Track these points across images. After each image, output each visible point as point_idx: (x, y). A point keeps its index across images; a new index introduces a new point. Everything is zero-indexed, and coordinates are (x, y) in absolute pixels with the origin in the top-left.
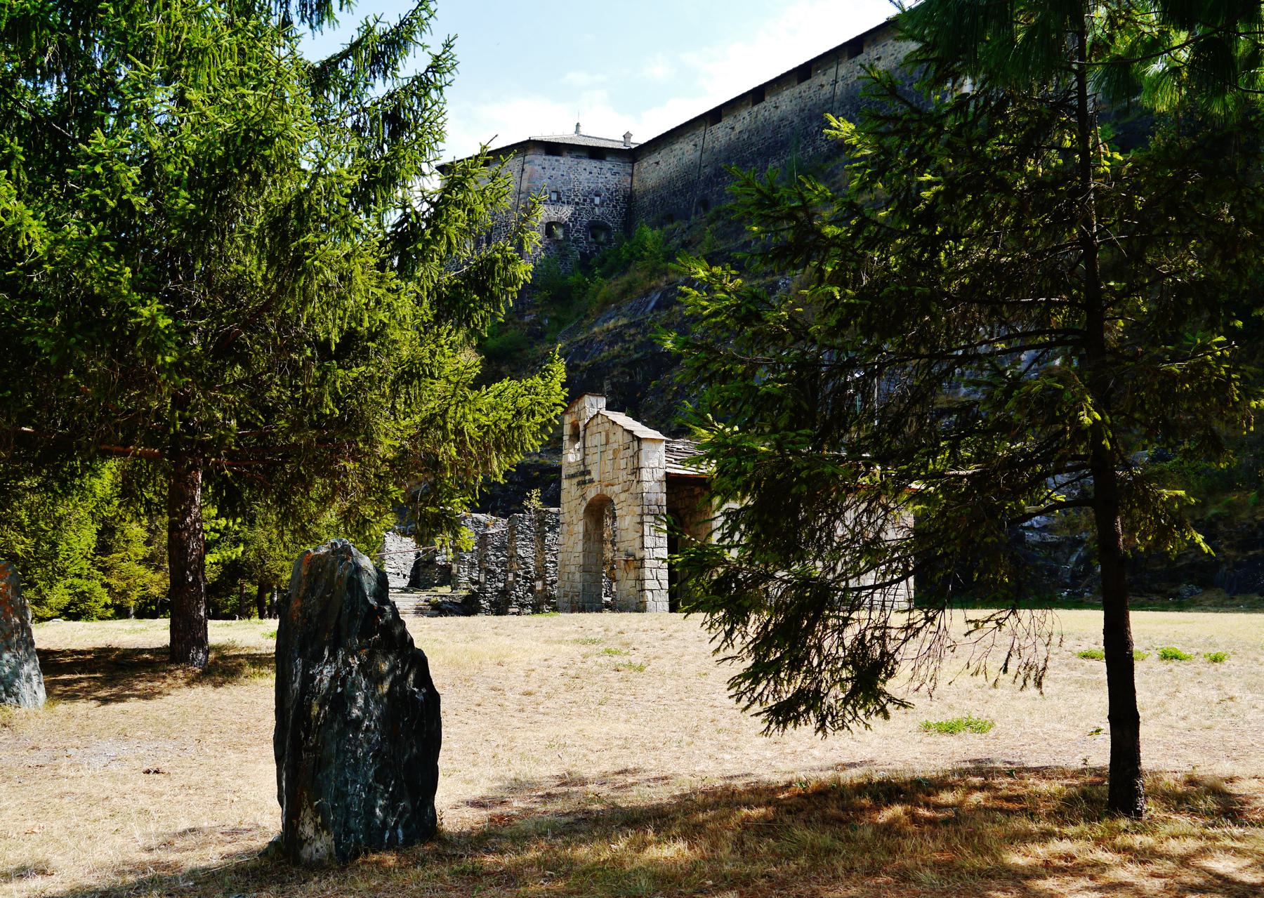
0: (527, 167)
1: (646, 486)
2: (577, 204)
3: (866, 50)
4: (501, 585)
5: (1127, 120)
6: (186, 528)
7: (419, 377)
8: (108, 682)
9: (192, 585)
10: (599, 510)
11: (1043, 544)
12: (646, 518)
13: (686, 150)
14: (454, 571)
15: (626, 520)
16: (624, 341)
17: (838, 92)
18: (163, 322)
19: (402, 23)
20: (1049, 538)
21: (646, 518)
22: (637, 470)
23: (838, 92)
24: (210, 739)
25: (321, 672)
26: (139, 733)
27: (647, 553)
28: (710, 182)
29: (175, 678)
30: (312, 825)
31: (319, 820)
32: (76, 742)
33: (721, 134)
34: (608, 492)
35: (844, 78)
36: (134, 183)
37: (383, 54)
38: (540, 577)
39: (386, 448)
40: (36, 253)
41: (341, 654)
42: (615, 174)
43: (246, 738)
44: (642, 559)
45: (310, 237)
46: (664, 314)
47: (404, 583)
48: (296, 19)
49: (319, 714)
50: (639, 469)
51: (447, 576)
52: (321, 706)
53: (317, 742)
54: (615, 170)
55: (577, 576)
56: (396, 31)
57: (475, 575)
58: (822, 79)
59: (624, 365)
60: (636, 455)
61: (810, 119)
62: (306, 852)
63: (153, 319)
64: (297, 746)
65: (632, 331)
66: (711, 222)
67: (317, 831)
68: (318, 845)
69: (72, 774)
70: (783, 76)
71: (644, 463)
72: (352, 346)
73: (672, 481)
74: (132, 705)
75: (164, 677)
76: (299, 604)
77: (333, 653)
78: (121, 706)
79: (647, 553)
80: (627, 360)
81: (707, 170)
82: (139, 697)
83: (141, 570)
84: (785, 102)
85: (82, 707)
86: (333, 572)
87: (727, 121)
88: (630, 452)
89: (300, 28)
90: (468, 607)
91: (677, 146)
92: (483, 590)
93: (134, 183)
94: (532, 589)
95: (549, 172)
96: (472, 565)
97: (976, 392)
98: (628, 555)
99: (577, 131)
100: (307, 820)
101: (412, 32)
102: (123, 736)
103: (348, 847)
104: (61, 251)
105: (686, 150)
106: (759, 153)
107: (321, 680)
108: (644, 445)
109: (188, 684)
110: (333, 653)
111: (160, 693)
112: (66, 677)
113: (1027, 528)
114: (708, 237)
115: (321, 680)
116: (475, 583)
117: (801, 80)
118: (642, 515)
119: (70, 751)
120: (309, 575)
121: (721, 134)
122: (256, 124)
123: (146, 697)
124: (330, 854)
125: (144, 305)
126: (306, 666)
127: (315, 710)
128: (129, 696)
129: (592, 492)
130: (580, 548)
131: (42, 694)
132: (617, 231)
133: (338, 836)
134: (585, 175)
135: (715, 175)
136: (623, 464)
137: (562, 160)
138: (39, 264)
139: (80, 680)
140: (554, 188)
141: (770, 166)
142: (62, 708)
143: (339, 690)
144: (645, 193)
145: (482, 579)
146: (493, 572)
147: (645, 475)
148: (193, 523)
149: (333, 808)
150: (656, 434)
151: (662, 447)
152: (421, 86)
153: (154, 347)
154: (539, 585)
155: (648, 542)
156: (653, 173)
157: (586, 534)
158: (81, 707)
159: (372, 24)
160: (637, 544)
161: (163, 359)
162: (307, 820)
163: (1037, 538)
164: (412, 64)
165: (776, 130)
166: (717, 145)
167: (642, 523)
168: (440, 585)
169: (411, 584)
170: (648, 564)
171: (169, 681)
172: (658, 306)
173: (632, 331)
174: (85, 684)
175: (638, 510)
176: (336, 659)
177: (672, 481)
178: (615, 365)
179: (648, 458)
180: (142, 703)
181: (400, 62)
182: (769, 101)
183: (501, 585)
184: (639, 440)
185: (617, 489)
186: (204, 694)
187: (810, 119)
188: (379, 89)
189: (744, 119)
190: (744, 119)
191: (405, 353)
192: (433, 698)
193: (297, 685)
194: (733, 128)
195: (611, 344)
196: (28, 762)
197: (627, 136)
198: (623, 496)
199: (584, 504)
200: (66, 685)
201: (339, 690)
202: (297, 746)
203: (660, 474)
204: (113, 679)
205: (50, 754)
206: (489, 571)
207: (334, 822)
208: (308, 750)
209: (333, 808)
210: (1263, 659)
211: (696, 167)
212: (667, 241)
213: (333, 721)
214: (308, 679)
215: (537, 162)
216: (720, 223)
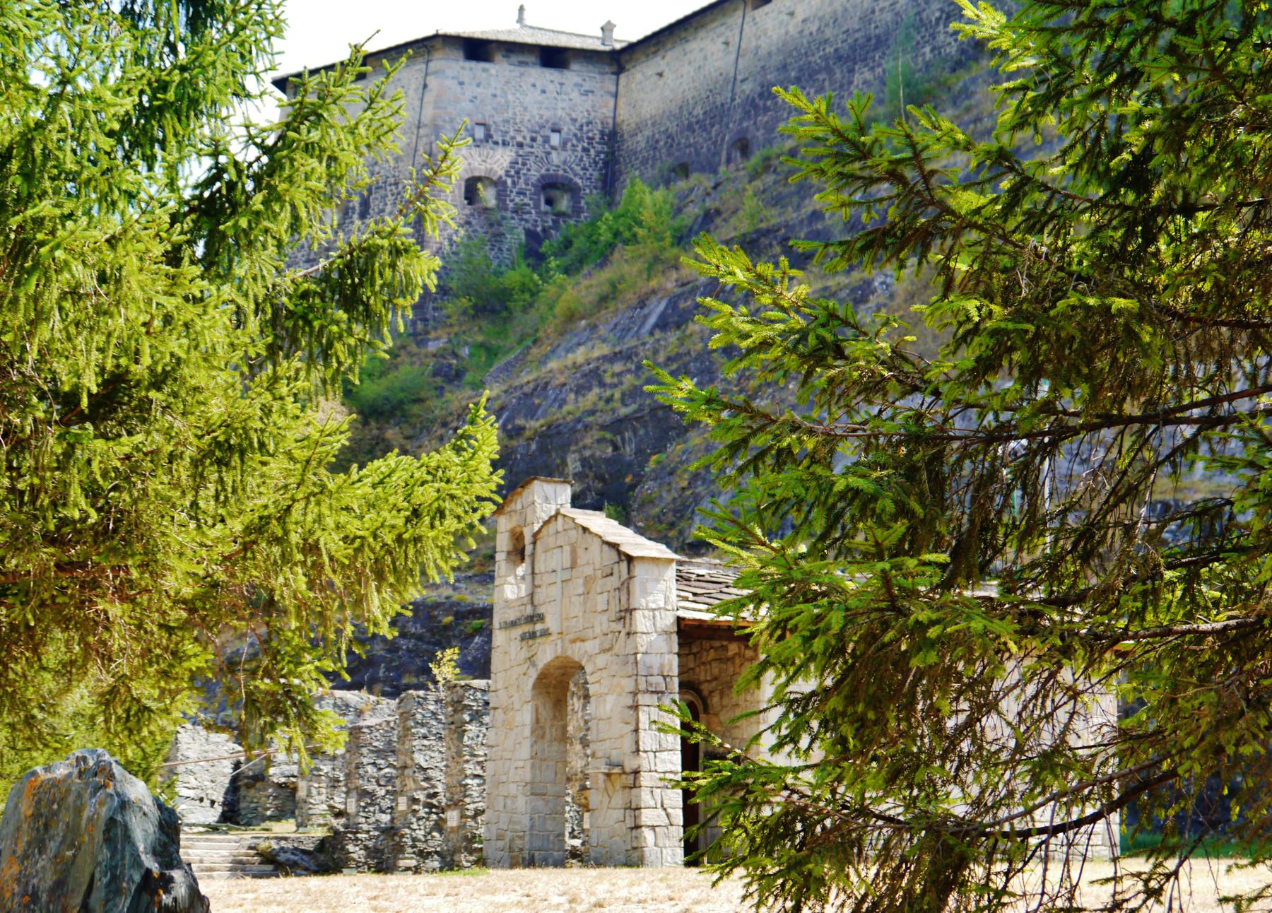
0: (432, 81)
1: (642, 642)
2: (520, 145)
10: (559, 685)
12: (643, 699)
14: (301, 793)
15: (606, 701)
16: (602, 384)
21: (643, 699)
22: (626, 613)
34: (576, 652)
38: (456, 804)
42: (586, 93)
44: (636, 772)
46: (673, 337)
47: (212, 816)
50: (630, 611)
51: (289, 802)
55: (522, 804)
57: (338, 802)
59: (603, 427)
60: (626, 587)
65: (618, 367)
66: (754, 176)
71: (639, 600)
73: (690, 635)
76: (15, 869)
80: (608, 418)
81: (748, 87)
86: (78, 811)
88: (613, 582)
90: (326, 859)
94: (439, 826)
95: (470, 91)
99: (520, 20)
106: (839, 58)
108: (638, 569)
116: (339, 814)
120: (36, 816)
130: (525, 751)
134: (532, 97)
136: (601, 602)
141: (857, 79)
145: (352, 808)
146: (371, 795)
147: (641, 621)
151: (671, 572)
154: (452, 818)
155: (648, 739)
157: (538, 728)
166: (764, 44)
167: (635, 707)
168: (277, 818)
170: (645, 779)
172: (662, 325)
175: (629, 684)
177: (690, 635)
178: (587, 427)
179: (645, 593)
184: (630, 559)
185: (591, 646)
195: (580, 390)
198: (601, 660)
199: (533, 675)
203: (668, 621)
206: (364, 794)
215: (449, 73)
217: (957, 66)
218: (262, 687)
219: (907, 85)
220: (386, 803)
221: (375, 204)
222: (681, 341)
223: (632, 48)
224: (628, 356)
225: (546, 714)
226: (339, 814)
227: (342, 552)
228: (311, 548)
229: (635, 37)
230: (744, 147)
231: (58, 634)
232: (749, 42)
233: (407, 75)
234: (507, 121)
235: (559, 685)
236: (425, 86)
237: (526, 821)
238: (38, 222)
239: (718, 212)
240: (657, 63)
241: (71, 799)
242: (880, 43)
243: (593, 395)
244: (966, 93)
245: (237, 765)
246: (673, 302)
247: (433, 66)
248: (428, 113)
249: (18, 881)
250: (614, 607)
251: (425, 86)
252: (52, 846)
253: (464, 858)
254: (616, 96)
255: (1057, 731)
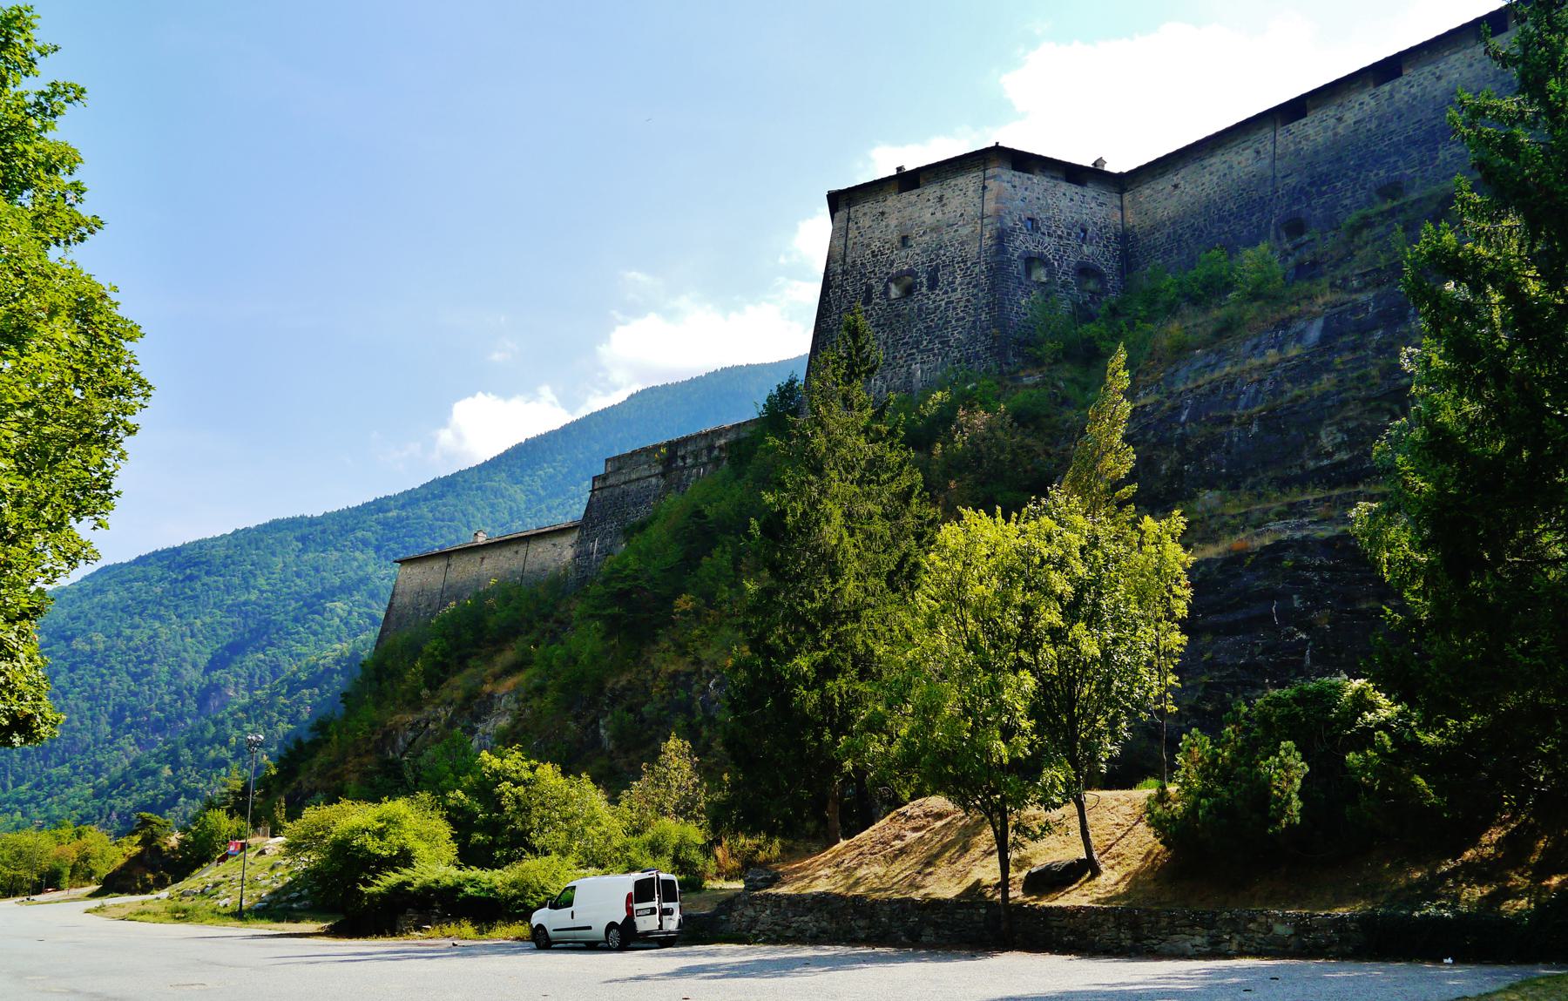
0: (991, 184)
2: (1060, 237)
42: (1101, 205)
54: (1101, 199)
95: (1021, 193)
112: (1235, 980)
132: (1112, 280)
134: (1064, 203)
135: (1311, 184)
140: (1029, 214)
144: (1154, 228)
156: (1162, 204)
182: (1409, 74)
194: (1340, 120)
210: (2, 556)
215: (1005, 177)
218: (102, 727)
221: (943, 278)
231: (490, 624)
233: (968, 182)
234: (1048, 219)
236: (984, 188)
247: (989, 172)
248: (990, 207)
251: (984, 188)
254: (1122, 209)
255: (946, 840)
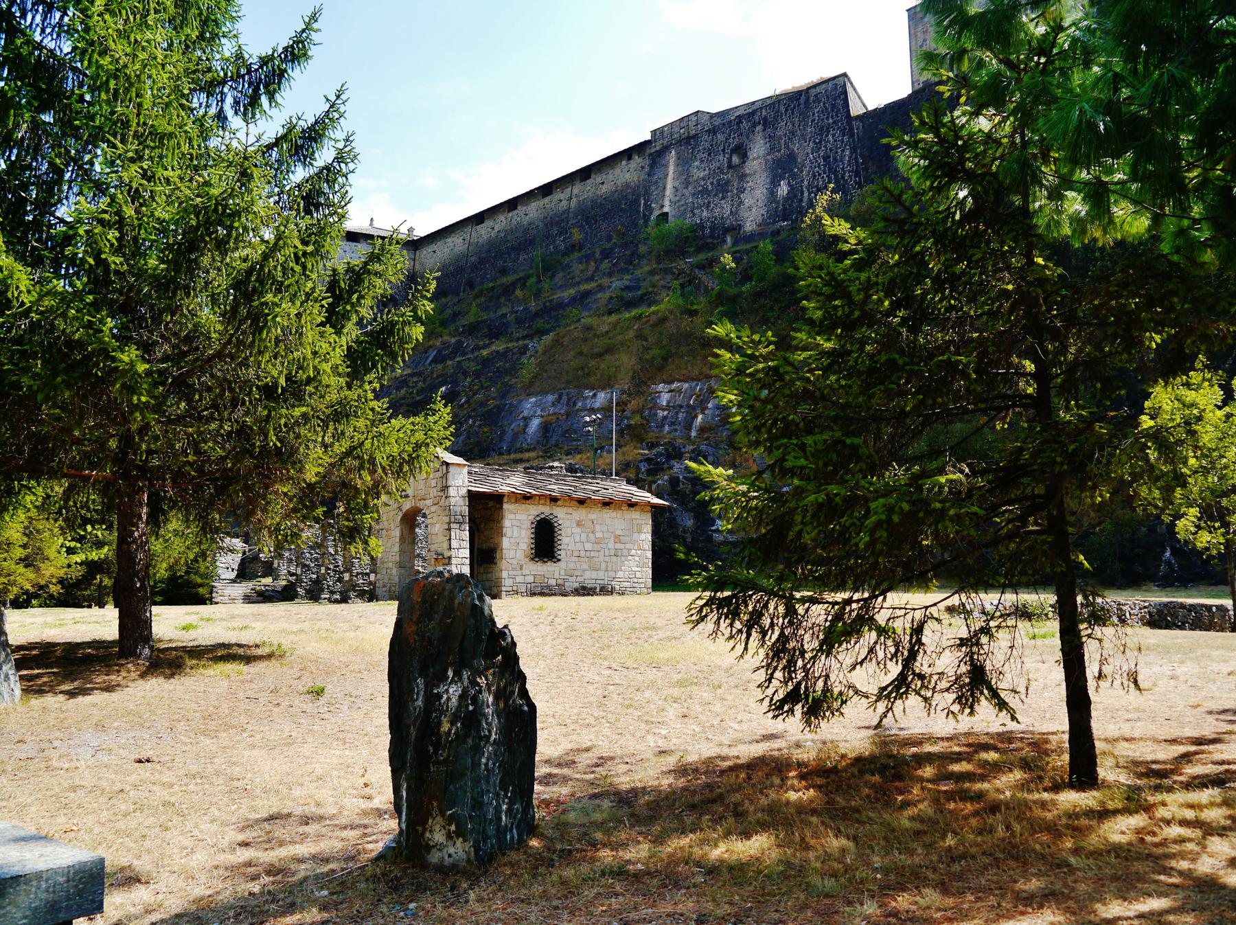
1: (453, 501)
3: (593, 176)
4: (314, 576)
5: (779, 238)
6: (135, 541)
7: (347, 416)
8: (68, 676)
9: (139, 590)
10: (410, 520)
11: (726, 543)
12: (453, 526)
13: (456, 243)
14: (275, 566)
15: (434, 526)
16: (408, 386)
17: (573, 206)
18: (142, 367)
19: (317, 122)
20: (731, 538)
21: (453, 526)
22: (445, 488)
23: (573, 206)
24: (181, 726)
25: (447, 691)
26: (116, 724)
27: (453, 553)
28: (475, 268)
29: (129, 672)
30: (443, 832)
31: (453, 828)
32: (58, 734)
33: (483, 232)
34: (421, 504)
35: (577, 196)
36: (112, 245)
37: (302, 146)
38: (348, 570)
39: (311, 473)
40: (23, 304)
41: (465, 674)
43: (212, 725)
44: (450, 558)
45: (269, 297)
46: (440, 367)
47: (233, 575)
48: (229, 113)
49: (450, 730)
50: (447, 487)
51: (269, 570)
52: (452, 723)
53: (449, 756)
55: (394, 571)
56: (312, 128)
57: (292, 569)
58: (560, 196)
59: (408, 405)
60: (445, 476)
61: (552, 224)
62: (434, 857)
63: (132, 363)
64: (423, 760)
65: (415, 379)
66: (476, 297)
67: (449, 836)
68: (452, 850)
69: (67, 766)
70: (532, 191)
71: (451, 482)
72: (295, 390)
73: (473, 497)
74: (98, 697)
75: (118, 671)
76: (414, 628)
77: (458, 674)
78: (87, 699)
79: (453, 553)
80: (410, 401)
81: (473, 259)
82: (102, 689)
83: (21, 569)
84: (533, 211)
85: (52, 701)
86: (452, 599)
87: (488, 223)
88: (439, 474)
89: (235, 122)
90: (287, 594)
91: (449, 240)
92: (299, 580)
93: (112, 245)
94: (340, 580)
96: (290, 561)
97: (676, 430)
98: (438, 554)
99: (371, 224)
100: (437, 828)
101: (324, 129)
102: (100, 727)
103: (485, 852)
104: (48, 302)
105: (456, 243)
106: (513, 248)
107: (449, 699)
108: (451, 469)
109: (143, 676)
110: (458, 674)
111: (118, 685)
113: (715, 531)
114: (474, 309)
115: (449, 699)
116: (292, 575)
117: (545, 196)
118: (449, 523)
119: (56, 743)
120: (424, 601)
121: (483, 232)
122: (223, 199)
123: (109, 689)
124: (469, 861)
125: (123, 351)
126: (429, 686)
127: (445, 727)
128: (92, 689)
129: (407, 505)
130: (397, 548)
131: (18, 692)
133: (476, 842)
136: (433, 483)
137: (359, 245)
138: (26, 313)
139: (39, 676)
141: (521, 258)
142: (36, 702)
143: (471, 708)
145: (299, 572)
146: (308, 566)
147: (452, 491)
148: (141, 536)
149: (471, 816)
150: (460, 460)
151: (466, 470)
152: (329, 174)
153: (130, 389)
154: (347, 576)
155: (454, 544)
157: (402, 539)
158: (50, 700)
159: (294, 121)
160: (446, 545)
161: (139, 399)
162: (437, 828)
163: (721, 538)
164: (325, 156)
165: (526, 231)
166: (480, 240)
167: (449, 529)
168: (263, 576)
169: (238, 576)
170: (454, 561)
171: (123, 674)
172: (435, 361)
173: (415, 379)
174: (45, 679)
175: (446, 519)
176: (461, 679)
177: (473, 497)
178: (401, 405)
179: (454, 479)
180: (106, 695)
181: (316, 155)
182: (521, 209)
183: (314, 576)
184: (447, 464)
185: (429, 502)
186: (156, 685)
187: (552, 224)
188: (299, 174)
189: (501, 223)
190: (501, 223)
191: (333, 396)
192: (533, 708)
193: (420, 703)
195: (398, 389)
196: (17, 755)
197: (411, 230)
198: (433, 509)
199: (401, 514)
200: (29, 681)
201: (471, 708)
202: (423, 760)
203: (464, 491)
204: (71, 673)
205: (37, 747)
206: (304, 566)
207: (473, 830)
208: (438, 763)
209: (471, 816)
211: (464, 256)
212: (442, 311)
213: (466, 736)
214: (432, 699)
216: (483, 299)
217: (564, 254)
219: (543, 261)
220: (315, 570)
222: (444, 368)
223: (422, 239)
224: (419, 374)
225: (406, 532)
226: (292, 575)
227: (385, 463)
228: (372, 461)
229: (423, 235)
230: (471, 285)
232: (474, 239)
235: (410, 520)
237: (397, 579)
238: (266, 304)
239: (460, 313)
240: (433, 247)
241: (446, 593)
242: (532, 242)
243: (403, 391)
244: (568, 266)
245: (244, 553)
246: (439, 352)
249: (417, 634)
250: (440, 485)
252: (437, 617)
253: (352, 594)
